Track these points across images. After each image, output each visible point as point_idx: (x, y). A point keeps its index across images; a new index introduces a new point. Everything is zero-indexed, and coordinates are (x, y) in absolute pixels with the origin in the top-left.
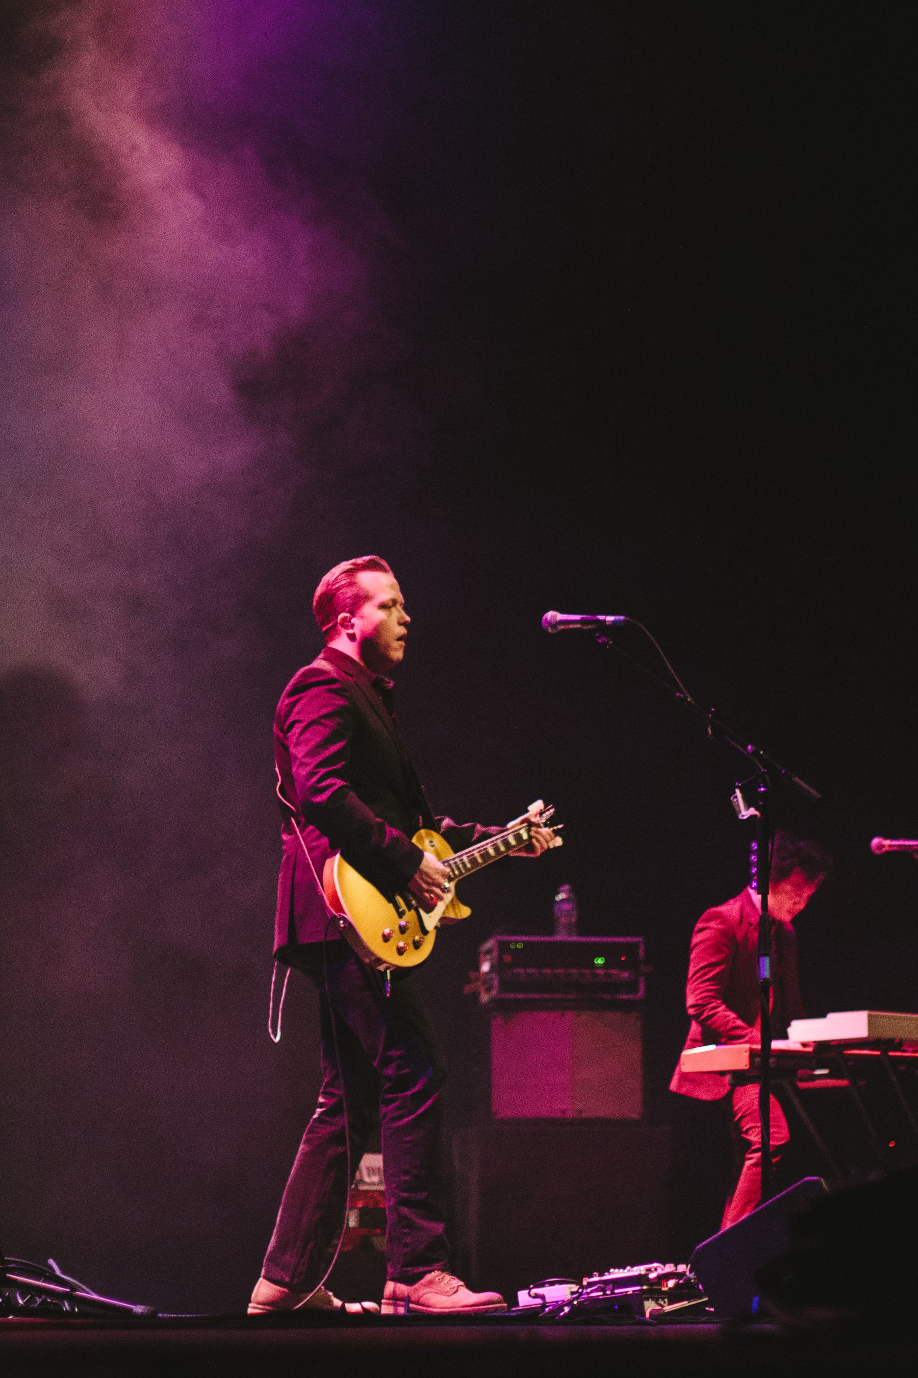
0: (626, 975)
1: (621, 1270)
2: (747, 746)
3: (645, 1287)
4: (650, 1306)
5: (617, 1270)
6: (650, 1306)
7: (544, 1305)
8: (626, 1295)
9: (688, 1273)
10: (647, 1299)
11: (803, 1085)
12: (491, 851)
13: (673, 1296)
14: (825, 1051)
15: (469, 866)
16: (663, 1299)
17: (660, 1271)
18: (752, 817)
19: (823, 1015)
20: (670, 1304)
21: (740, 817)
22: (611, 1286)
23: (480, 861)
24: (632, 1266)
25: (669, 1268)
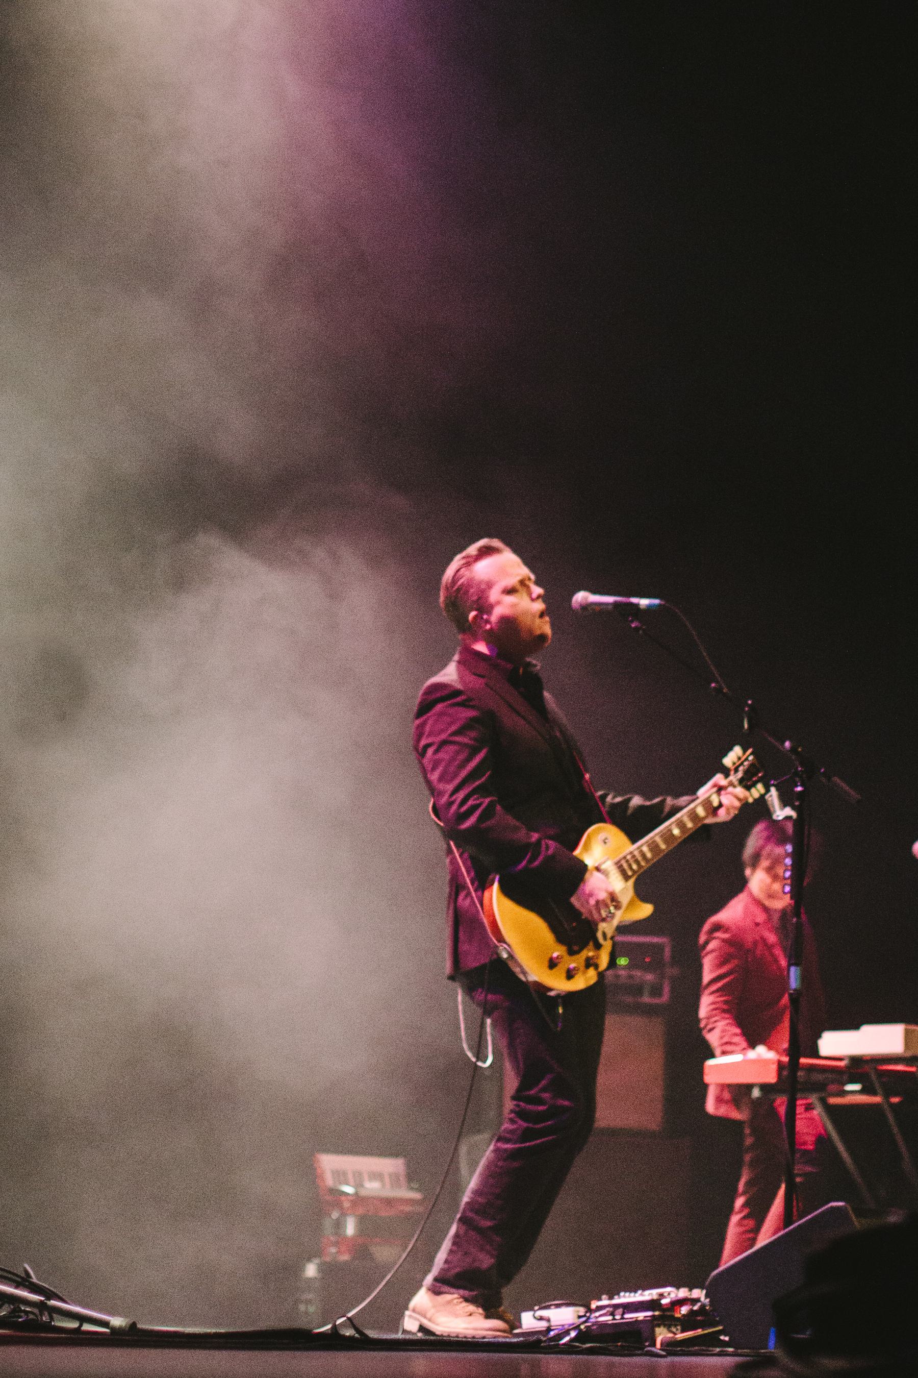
0: (649, 977)
1: (632, 1294)
2: (784, 742)
3: (657, 1313)
4: (662, 1334)
5: (627, 1294)
6: (662, 1334)
7: (549, 1329)
8: (637, 1322)
9: (703, 1299)
10: (659, 1326)
11: (833, 1101)
12: (676, 832)
13: (688, 1323)
14: (858, 1067)
15: (649, 855)
16: (676, 1326)
17: (673, 1295)
18: (788, 818)
19: (856, 1026)
20: (682, 1332)
21: (774, 817)
22: (620, 1310)
23: (663, 846)
24: (644, 1289)
25: (683, 1293)
